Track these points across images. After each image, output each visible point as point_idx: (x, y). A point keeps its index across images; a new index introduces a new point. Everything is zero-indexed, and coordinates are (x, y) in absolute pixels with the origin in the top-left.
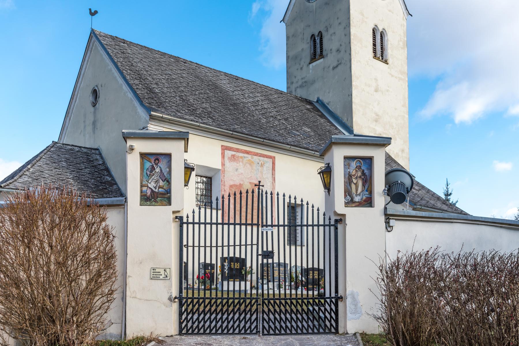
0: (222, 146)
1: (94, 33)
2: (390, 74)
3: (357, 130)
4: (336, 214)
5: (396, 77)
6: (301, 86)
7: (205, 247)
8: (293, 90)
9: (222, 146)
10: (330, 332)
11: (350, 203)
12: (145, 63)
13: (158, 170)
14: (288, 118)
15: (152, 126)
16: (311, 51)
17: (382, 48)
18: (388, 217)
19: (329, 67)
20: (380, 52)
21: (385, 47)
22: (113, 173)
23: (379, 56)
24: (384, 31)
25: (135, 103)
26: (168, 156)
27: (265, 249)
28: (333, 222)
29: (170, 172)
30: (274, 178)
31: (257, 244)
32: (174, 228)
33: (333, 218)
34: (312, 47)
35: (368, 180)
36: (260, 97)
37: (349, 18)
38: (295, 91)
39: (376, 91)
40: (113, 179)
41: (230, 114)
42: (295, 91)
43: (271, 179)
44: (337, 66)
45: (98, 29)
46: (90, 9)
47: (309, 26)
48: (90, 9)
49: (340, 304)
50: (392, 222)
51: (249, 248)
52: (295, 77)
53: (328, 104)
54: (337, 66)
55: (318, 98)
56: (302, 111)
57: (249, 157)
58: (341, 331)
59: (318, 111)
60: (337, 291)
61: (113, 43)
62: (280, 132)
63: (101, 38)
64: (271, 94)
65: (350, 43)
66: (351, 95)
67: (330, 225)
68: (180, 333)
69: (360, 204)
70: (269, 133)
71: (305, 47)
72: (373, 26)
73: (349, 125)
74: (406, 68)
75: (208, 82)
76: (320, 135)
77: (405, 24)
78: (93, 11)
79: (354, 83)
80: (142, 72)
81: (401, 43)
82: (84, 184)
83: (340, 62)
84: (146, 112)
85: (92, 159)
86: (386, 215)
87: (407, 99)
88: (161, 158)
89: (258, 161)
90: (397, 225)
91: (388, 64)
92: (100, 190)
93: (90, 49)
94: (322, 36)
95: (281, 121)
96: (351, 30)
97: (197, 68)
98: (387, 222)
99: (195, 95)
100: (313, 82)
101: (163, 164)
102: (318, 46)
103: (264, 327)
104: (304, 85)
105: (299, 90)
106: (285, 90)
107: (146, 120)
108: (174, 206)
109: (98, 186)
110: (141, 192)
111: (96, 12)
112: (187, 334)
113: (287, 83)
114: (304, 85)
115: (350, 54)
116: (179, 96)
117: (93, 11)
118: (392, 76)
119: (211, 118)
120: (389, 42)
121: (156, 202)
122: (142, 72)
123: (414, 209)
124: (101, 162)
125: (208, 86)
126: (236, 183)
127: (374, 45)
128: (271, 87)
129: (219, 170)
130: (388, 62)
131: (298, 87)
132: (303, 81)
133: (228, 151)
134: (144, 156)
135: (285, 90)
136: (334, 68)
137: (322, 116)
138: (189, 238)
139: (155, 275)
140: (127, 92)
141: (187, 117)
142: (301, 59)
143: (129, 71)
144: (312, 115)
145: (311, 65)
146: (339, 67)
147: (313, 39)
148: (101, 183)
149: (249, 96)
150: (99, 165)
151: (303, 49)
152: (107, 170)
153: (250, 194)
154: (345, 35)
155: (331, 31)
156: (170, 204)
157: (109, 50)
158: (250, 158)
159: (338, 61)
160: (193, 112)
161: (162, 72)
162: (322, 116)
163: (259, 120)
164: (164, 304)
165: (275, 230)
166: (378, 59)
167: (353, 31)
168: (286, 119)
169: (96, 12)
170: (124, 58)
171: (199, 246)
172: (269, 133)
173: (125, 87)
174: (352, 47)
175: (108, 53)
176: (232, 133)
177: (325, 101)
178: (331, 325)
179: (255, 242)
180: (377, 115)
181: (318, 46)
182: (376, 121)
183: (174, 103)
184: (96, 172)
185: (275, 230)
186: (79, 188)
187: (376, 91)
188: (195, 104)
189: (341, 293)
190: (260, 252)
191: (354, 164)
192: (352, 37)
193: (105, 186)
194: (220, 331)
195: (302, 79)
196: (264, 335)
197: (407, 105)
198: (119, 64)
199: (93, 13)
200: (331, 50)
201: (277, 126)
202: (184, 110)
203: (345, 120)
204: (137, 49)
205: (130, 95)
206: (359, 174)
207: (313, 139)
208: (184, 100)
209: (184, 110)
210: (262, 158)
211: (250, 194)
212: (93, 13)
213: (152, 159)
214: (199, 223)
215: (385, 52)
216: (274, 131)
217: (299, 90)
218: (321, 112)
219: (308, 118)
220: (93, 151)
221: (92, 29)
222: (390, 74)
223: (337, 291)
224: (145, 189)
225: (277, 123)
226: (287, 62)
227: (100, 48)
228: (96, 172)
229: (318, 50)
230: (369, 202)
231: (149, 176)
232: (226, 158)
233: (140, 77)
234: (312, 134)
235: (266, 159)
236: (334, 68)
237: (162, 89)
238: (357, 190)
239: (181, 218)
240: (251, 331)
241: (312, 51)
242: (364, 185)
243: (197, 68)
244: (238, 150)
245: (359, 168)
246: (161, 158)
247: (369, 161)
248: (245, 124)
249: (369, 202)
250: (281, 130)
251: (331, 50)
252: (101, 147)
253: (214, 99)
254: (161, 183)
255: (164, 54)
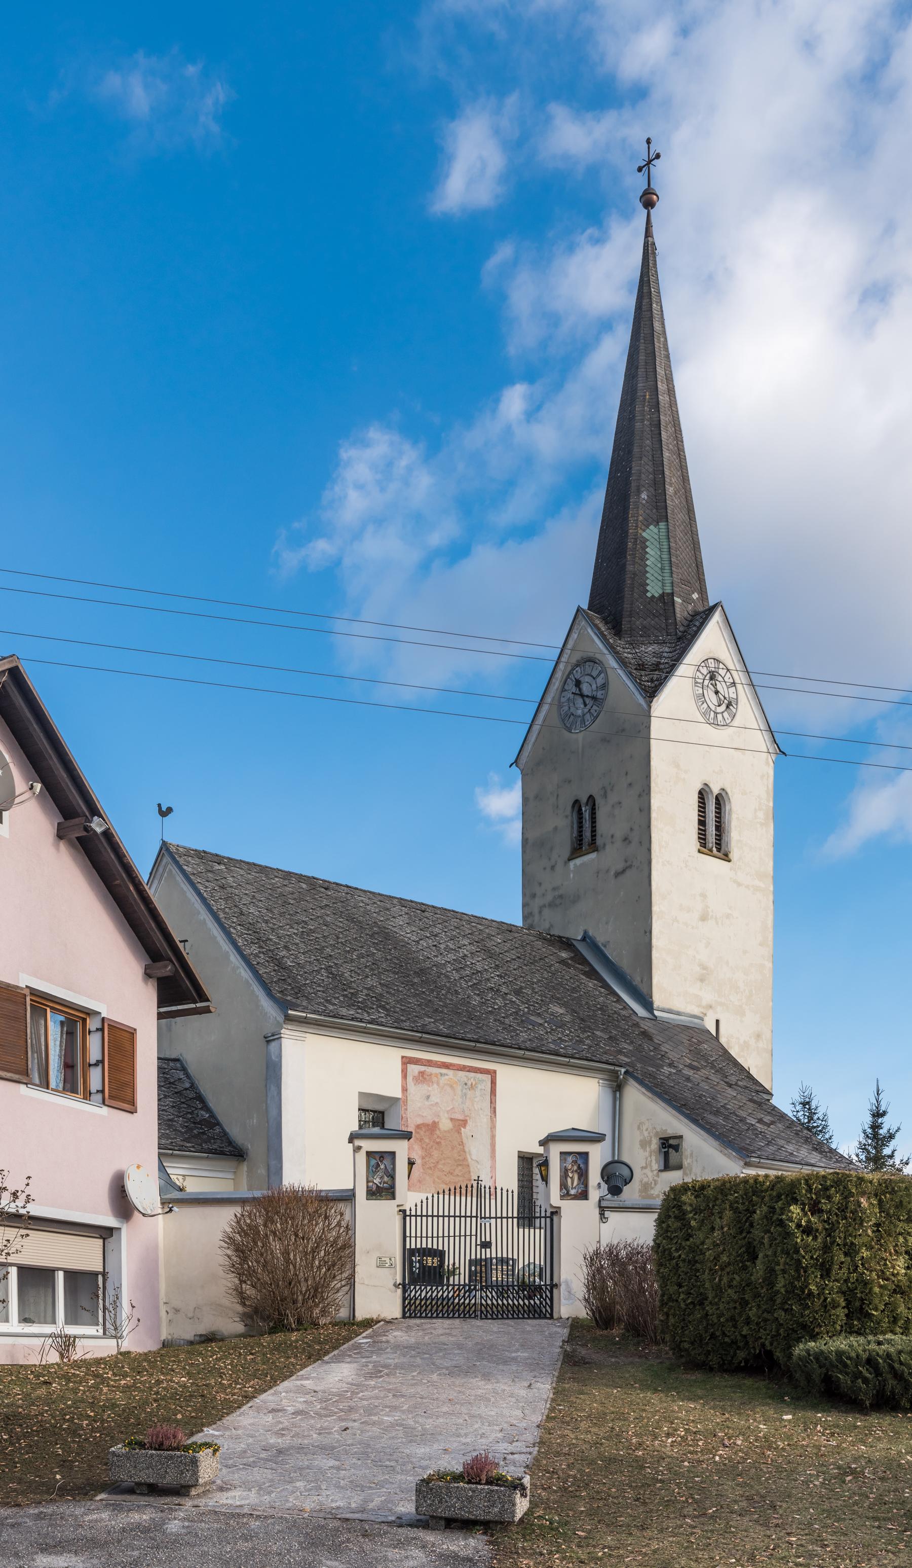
0: (403, 1057)
1: (168, 849)
2: (735, 881)
3: (659, 999)
4: (551, 1206)
5: (747, 887)
6: (552, 905)
7: (427, 1237)
8: (536, 911)
9: (403, 1057)
10: (545, 1318)
11: (566, 1195)
12: (260, 904)
13: (382, 1167)
14: (521, 988)
15: (288, 1032)
16: (572, 833)
17: (719, 828)
18: (602, 1210)
19: (608, 871)
20: (713, 833)
21: (726, 818)
22: (211, 1105)
23: (710, 845)
24: (724, 794)
25: (256, 989)
26: (393, 1154)
27: (483, 1240)
28: (548, 1214)
29: (394, 1169)
30: (495, 1108)
31: (476, 1235)
32: (398, 1219)
33: (549, 1210)
34: (575, 826)
35: (583, 1174)
36: (469, 948)
37: (648, 777)
38: (540, 912)
39: (704, 918)
40: (212, 1116)
41: (415, 995)
42: (540, 912)
43: (488, 1111)
44: (623, 871)
45: (172, 840)
46: (159, 805)
47: (570, 781)
48: (159, 805)
49: (555, 1291)
50: (607, 1214)
51: (463, 1238)
52: (540, 884)
53: (605, 946)
54: (623, 871)
55: (585, 932)
56: (550, 967)
57: (450, 1073)
58: (555, 1316)
59: (584, 961)
60: (552, 1279)
61: (201, 868)
62: (507, 1021)
63: (181, 861)
64: (489, 936)
65: (649, 827)
66: (649, 932)
67: (546, 1217)
68: (404, 1317)
69: (576, 1197)
70: (485, 1028)
71: (560, 824)
72: (699, 786)
73: (645, 991)
74: (771, 864)
75: (372, 928)
76: (582, 1020)
77: (771, 773)
78: (164, 809)
79: (655, 909)
80: (259, 925)
81: (761, 815)
82: (170, 1126)
83: (628, 864)
84: (279, 1011)
85: (172, 1080)
86: (600, 1207)
87: (771, 930)
88: (385, 1155)
89: (466, 1080)
90: (612, 1216)
91: (729, 861)
92: (195, 1136)
93: (158, 876)
94: (594, 805)
95: (509, 997)
96: (652, 801)
97: (349, 897)
98: (602, 1214)
99: (352, 960)
100: (576, 899)
101: (387, 1162)
102: (587, 825)
103: (482, 1312)
104: (558, 901)
105: (546, 912)
106: (519, 922)
107: (278, 1022)
108: (398, 1201)
109: (191, 1130)
110: (368, 1187)
111: (170, 810)
112: (410, 1317)
113: (524, 895)
114: (558, 901)
115: (649, 850)
116: (326, 969)
117: (164, 809)
118: (739, 884)
119: (384, 1008)
120: (734, 816)
121: (381, 1196)
122: (259, 925)
123: (747, 1165)
124: (187, 1085)
125: (372, 936)
126: (426, 1122)
127: (702, 823)
128: (489, 918)
129: (396, 1100)
130: (731, 856)
131: (544, 906)
132: (557, 893)
133: (413, 1066)
134: (369, 1154)
135: (519, 922)
136: (617, 874)
137: (592, 974)
138: (411, 1230)
139: (381, 1265)
140: (238, 968)
141: (344, 1011)
142: (551, 849)
143: (239, 928)
144: (572, 975)
145: (572, 864)
146: (628, 873)
147: (576, 808)
148: (194, 1123)
149: (448, 949)
150: (186, 1089)
151: (556, 829)
152: (200, 1098)
153: (469, 1189)
154: (641, 810)
155: (613, 798)
156: (394, 1198)
157: (200, 887)
158: (451, 1076)
159: (626, 861)
160: (351, 1000)
161: (290, 919)
162: (592, 974)
163: (466, 1002)
164: (390, 1290)
165: (493, 1221)
166: (710, 853)
167: (657, 801)
168: (518, 992)
169: (170, 810)
170: (226, 899)
171: (427, 1237)
172: (485, 1028)
173: (234, 959)
174: (653, 835)
175: (199, 894)
176: (420, 1035)
177: (600, 939)
178: (546, 1311)
179: (474, 1233)
180: (704, 968)
181: (587, 825)
182: (702, 980)
183: (320, 986)
184: (183, 1103)
185: (493, 1221)
186: (163, 1134)
187: (704, 918)
188: (354, 982)
189: (555, 1281)
190: (479, 1243)
191: (570, 1159)
192: (654, 815)
193: (201, 1128)
194: (440, 1315)
195: (554, 889)
196: (481, 1319)
197: (770, 943)
198: (222, 915)
199: (165, 812)
200: (612, 836)
201: (499, 1008)
202: (338, 998)
203: (637, 980)
204: (242, 872)
205: (245, 973)
206: (575, 1168)
207: (569, 1030)
208: (334, 977)
209: (338, 998)
210: (472, 1074)
211: (469, 1189)
212: (165, 812)
213: (378, 1157)
214: (422, 1216)
215: (724, 838)
216: (495, 1020)
217: (546, 912)
218: (590, 965)
219: (561, 984)
220: (171, 1064)
221: (164, 842)
222: (735, 881)
223: (552, 1279)
224: (370, 1184)
225: (500, 1002)
226: (524, 852)
227: (180, 878)
228: (183, 1103)
229: (587, 834)
230: (584, 1195)
231: (375, 1173)
232: (410, 1079)
233: (260, 940)
234: (568, 1018)
235: (479, 1076)
236: (617, 874)
237: (296, 957)
238: (572, 1184)
239: (404, 1211)
240: (470, 1315)
241: (575, 834)
242: (579, 1179)
243: (349, 897)
244: (430, 1063)
245: (575, 1162)
246: (385, 1155)
247: (585, 1156)
248: (442, 1012)
249: (584, 1195)
250: (507, 1017)
251: (612, 836)
252: (184, 1056)
253: (384, 966)
254: (386, 1179)
255: (288, 875)
